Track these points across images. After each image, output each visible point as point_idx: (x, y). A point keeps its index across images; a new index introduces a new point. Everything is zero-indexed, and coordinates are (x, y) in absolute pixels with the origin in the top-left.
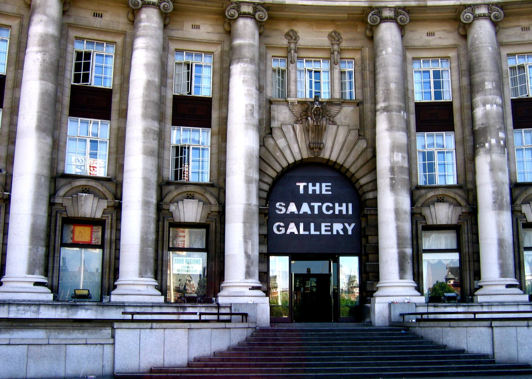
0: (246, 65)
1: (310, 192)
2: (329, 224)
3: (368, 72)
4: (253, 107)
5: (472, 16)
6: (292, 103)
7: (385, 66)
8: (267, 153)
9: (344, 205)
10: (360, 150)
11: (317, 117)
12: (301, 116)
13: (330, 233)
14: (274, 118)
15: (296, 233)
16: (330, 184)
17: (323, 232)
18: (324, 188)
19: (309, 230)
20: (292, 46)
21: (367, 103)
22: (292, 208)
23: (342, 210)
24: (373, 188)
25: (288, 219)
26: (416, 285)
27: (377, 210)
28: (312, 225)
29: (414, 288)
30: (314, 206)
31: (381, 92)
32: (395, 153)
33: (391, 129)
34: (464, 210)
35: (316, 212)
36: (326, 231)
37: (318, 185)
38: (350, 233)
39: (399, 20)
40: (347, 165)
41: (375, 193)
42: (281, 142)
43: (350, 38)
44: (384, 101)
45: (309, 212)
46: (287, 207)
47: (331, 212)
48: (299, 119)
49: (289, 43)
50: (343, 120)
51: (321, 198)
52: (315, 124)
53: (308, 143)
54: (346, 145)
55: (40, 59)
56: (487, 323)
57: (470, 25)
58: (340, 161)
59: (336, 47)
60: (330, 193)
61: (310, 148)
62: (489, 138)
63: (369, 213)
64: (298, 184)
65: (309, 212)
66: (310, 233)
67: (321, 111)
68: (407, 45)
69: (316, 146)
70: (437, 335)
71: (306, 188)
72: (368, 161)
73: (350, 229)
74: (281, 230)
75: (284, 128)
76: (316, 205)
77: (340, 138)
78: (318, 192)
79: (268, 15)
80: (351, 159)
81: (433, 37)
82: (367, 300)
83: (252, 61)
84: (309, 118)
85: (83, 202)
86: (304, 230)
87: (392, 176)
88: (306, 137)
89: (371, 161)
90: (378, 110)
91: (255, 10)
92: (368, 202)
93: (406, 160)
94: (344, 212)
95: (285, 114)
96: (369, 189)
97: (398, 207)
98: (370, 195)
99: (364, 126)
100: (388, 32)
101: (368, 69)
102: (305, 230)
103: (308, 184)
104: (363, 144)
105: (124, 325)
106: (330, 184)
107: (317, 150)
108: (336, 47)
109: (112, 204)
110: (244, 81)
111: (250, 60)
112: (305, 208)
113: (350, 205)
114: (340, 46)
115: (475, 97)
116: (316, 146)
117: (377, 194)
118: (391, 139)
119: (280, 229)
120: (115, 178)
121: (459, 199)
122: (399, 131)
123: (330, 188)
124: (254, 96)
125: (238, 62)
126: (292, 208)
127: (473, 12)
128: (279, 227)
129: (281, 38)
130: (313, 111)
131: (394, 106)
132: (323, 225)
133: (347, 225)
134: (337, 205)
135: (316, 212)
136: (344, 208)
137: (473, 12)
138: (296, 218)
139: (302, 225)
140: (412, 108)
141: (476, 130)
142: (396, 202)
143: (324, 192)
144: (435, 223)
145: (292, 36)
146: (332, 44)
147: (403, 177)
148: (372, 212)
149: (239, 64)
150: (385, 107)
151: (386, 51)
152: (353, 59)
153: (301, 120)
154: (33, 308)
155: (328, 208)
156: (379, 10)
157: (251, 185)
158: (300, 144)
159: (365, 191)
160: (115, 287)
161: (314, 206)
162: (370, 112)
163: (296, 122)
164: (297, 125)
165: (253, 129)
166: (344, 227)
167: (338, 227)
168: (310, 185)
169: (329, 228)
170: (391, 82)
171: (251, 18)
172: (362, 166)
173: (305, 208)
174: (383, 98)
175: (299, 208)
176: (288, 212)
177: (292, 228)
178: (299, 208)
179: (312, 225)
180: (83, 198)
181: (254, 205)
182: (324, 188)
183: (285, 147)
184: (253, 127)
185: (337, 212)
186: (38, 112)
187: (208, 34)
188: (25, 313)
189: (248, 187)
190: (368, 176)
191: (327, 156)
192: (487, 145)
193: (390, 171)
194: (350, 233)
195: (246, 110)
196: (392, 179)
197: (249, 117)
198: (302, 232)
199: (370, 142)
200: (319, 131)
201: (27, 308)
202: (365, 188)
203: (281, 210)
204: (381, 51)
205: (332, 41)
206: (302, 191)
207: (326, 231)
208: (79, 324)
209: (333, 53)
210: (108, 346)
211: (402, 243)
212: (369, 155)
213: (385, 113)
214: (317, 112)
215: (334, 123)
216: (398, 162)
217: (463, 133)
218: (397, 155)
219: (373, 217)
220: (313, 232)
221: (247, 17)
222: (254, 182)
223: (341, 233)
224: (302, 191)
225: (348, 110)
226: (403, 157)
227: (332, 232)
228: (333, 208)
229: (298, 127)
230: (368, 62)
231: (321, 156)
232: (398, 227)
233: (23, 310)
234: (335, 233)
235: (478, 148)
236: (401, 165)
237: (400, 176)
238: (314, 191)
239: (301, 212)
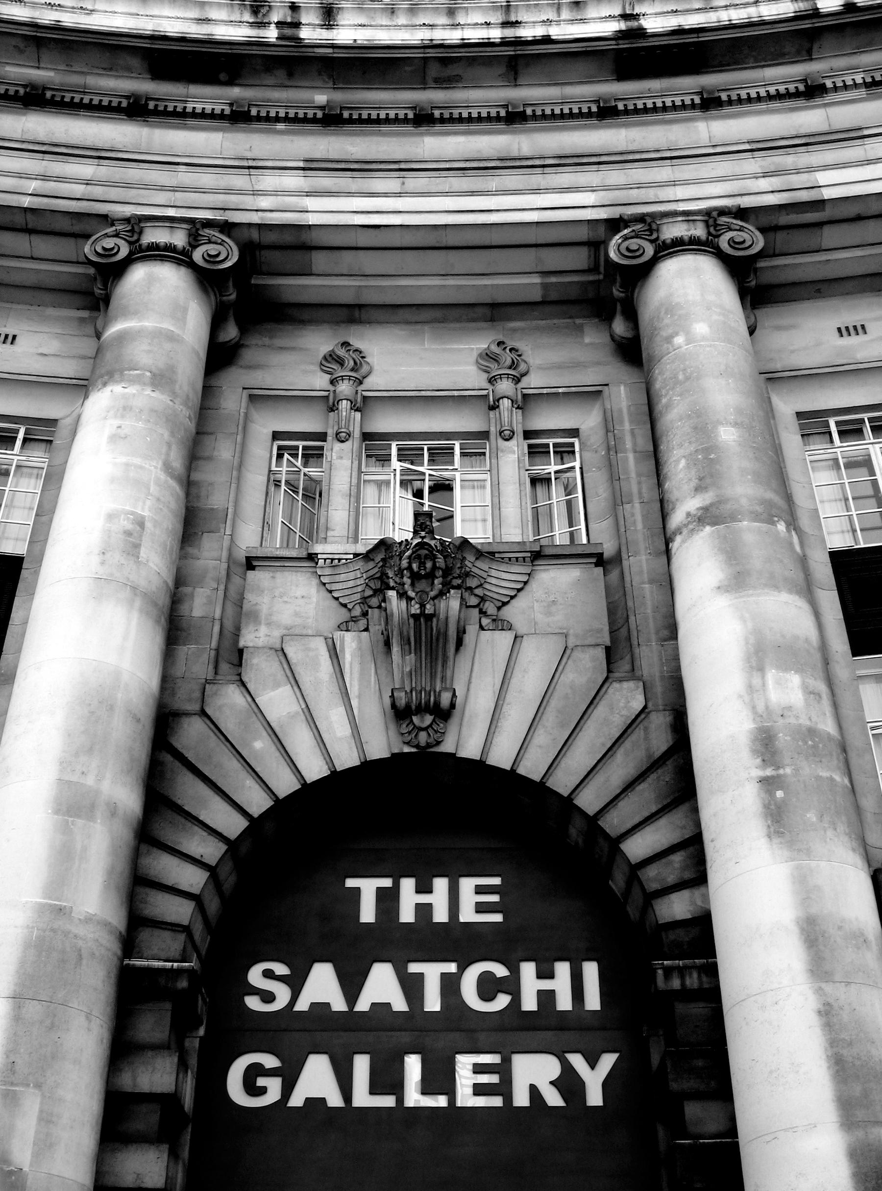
0: (132, 390)
1: (407, 915)
3: (631, 456)
4: (141, 523)
6: (334, 562)
7: (687, 379)
8: (213, 741)
9: (563, 969)
11: (422, 585)
13: (496, 1102)
14: (254, 617)
16: (496, 881)
17: (466, 1098)
19: (397, 1088)
21: (636, 554)
22: (323, 985)
23: (552, 993)
24: (688, 875)
25: (297, 1035)
27: (712, 971)
28: (413, 1065)
30: (421, 976)
31: (683, 463)
32: (771, 675)
33: (738, 580)
35: (433, 1002)
36: (479, 1090)
37: (441, 885)
38: (595, 1098)
40: (562, 783)
41: (697, 892)
42: (278, 702)
43: (556, 358)
44: (699, 489)
47: (502, 1001)
48: (357, 611)
50: (539, 617)
51: (455, 942)
52: (415, 609)
54: (555, 703)
58: (532, 768)
60: (498, 918)
61: (401, 714)
63: (676, 984)
64: (351, 883)
65: (400, 1004)
66: (400, 1100)
67: (440, 561)
68: (771, 367)
69: (422, 710)
71: (388, 900)
72: (655, 765)
73: (594, 1081)
74: (263, 1091)
75: (290, 651)
76: (432, 973)
77: (530, 680)
78: (441, 915)
79: (237, 244)
80: (580, 758)
81: (862, 338)
83: (161, 379)
86: (375, 1089)
87: (769, 772)
89: (670, 764)
90: (678, 531)
91: (195, 240)
93: (826, 704)
94: (564, 1003)
95: (301, 602)
96: (672, 879)
97: (814, 910)
98: (677, 907)
99: (629, 638)
100: (691, 295)
101: (629, 445)
103: (396, 887)
104: (627, 699)
106: (496, 881)
107: (428, 719)
108: (505, 386)
110: (114, 438)
111: (154, 375)
113: (591, 971)
114: (522, 384)
116: (422, 710)
117: (706, 898)
118: (743, 619)
119: (261, 1082)
122: (776, 587)
123: (495, 898)
124: (153, 488)
126: (323, 985)
128: (253, 1072)
129: (305, 372)
130: (405, 563)
131: (744, 502)
132: (464, 1063)
133: (577, 1061)
134: (528, 970)
135: (433, 1002)
138: (335, 1033)
139: (362, 1065)
140: (824, 571)
142: (805, 889)
143: (468, 915)
145: (344, 363)
146: (492, 381)
147: (825, 774)
148: (693, 981)
149: (108, 389)
150: (706, 509)
151: (688, 333)
153: (365, 614)
155: (488, 987)
156: (648, 223)
157: (80, 822)
158: (355, 703)
161: (421, 976)
162: (651, 581)
163: (344, 627)
164: (348, 636)
165: (131, 603)
166: (568, 1070)
167: (535, 1073)
168: (408, 885)
169: (494, 1079)
170: (719, 422)
171: (179, 262)
172: (629, 787)
173: (382, 986)
174: (694, 483)
175: (352, 985)
177: (317, 1079)
178: (352, 985)
179: (413, 1065)
181: (88, 920)
182: (468, 899)
183: (292, 716)
184: (127, 593)
185: (529, 1003)
187: (41, 358)
189: (65, 829)
190: (663, 822)
191: (470, 750)
193: (755, 752)
194: (595, 1098)
195: (108, 533)
196: (768, 784)
197: (116, 557)
198: (362, 1098)
199: (659, 689)
200: (432, 644)
202: (653, 876)
203: (268, 997)
204: (669, 339)
206: (368, 914)
207: (479, 1090)
211: (866, 1094)
212: (660, 740)
213: (708, 529)
214: (422, 564)
215: (501, 625)
216: (790, 708)
218: (778, 682)
219: (698, 1009)
220: (414, 1098)
221: (162, 259)
222: (100, 813)
223: (553, 1099)
224: (368, 914)
225: (557, 581)
226: (809, 692)
227: (508, 1096)
228: (512, 986)
229: (351, 644)
230: (627, 426)
231: (447, 747)
232: (828, 1014)
234: (521, 1099)
236: (804, 721)
237: (808, 769)
238: (424, 911)
239: (363, 1005)
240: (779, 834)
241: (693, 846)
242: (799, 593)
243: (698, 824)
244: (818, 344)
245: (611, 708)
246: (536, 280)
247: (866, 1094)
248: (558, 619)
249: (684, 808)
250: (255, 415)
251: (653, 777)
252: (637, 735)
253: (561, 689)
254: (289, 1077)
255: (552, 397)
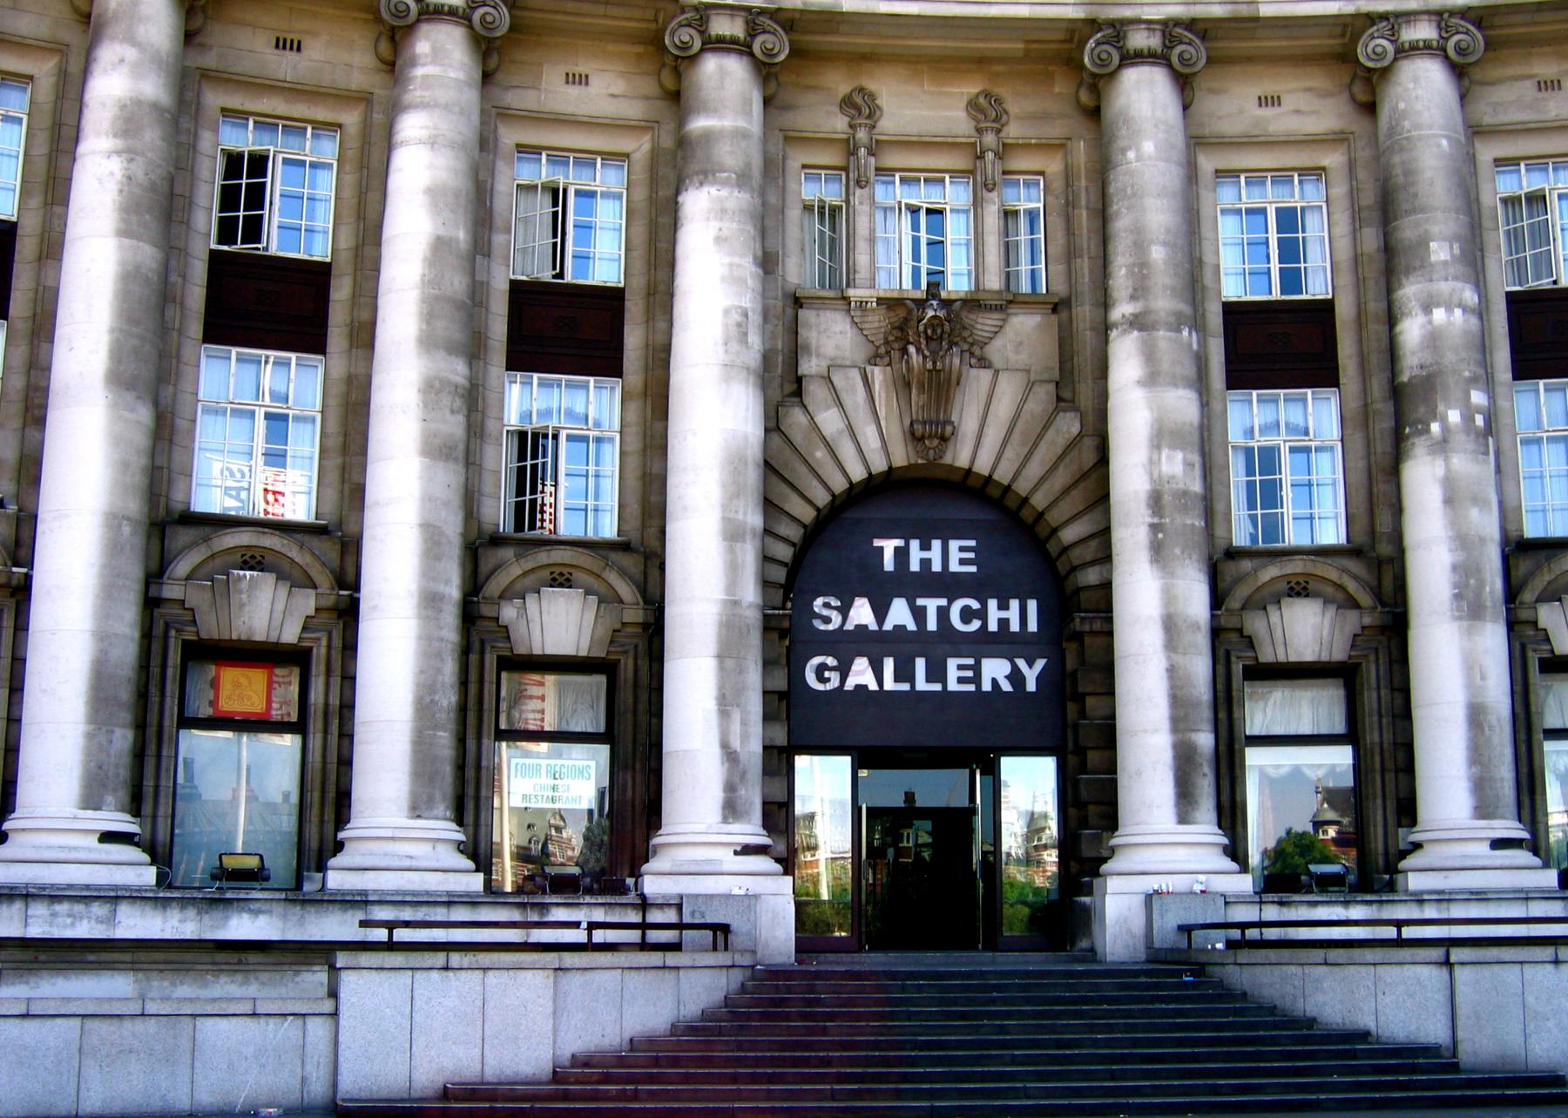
0: (725, 192)
1: (915, 566)
2: (971, 661)
3: (1084, 213)
4: (746, 315)
5: (1390, 48)
6: (862, 304)
7: (1134, 195)
8: (788, 452)
9: (1014, 604)
10: (1061, 442)
11: (934, 345)
12: (887, 342)
13: (971, 688)
14: (807, 349)
15: (873, 686)
16: (972, 543)
17: (953, 685)
18: (955, 555)
20: (862, 135)
21: (1082, 304)
22: (862, 613)
25: (848, 645)
26: (1225, 841)
27: (1110, 620)
28: (920, 664)
29: (1219, 850)
30: (924, 608)
31: (1123, 271)
32: (1165, 452)
33: (1151, 379)
34: (1367, 621)
35: (932, 625)
36: (961, 680)
37: (936, 544)
38: (1031, 686)
39: (1175, 60)
40: (1022, 487)
41: (1105, 568)
42: (829, 420)
43: (1031, 111)
45: (912, 626)
46: (844, 611)
47: (976, 625)
48: (882, 350)
49: (851, 126)
50: (1011, 355)
51: (947, 585)
52: (929, 365)
53: (907, 422)
54: (1019, 426)
55: (119, 175)
56: (1436, 953)
57: (1385, 72)
58: (1003, 475)
59: (989, 139)
60: (973, 569)
61: (914, 437)
62: (1441, 408)
63: (1087, 628)
64: (877, 543)
65: (911, 626)
67: (947, 327)
68: (1198, 133)
69: (931, 431)
70: (1289, 989)
71: (902, 555)
72: (1084, 476)
73: (1031, 676)
74: (829, 680)
75: (836, 379)
76: (932, 605)
77: (1003, 408)
78: (937, 567)
80: (1035, 470)
82: (1082, 885)
83: (742, 180)
84: (912, 349)
85: (244, 596)
86: (897, 679)
87: (1156, 520)
88: (902, 404)
89: (1094, 476)
90: (1115, 325)
91: (753, 30)
92: (1084, 596)
93: (1197, 472)
94: (1015, 626)
96: (1089, 558)
97: (1172, 610)
98: (1091, 576)
99: (1072, 373)
100: (1144, 96)
101: (1083, 202)
102: (898, 678)
103: (907, 544)
104: (1069, 425)
105: (365, 958)
106: (972, 543)
107: (936, 442)
108: (989, 139)
109: (329, 601)
111: (738, 176)
112: (899, 614)
113: (1032, 605)
115: (1400, 286)
116: (931, 431)
117: (1110, 572)
118: (1151, 409)
119: (827, 674)
120: (340, 525)
121: (1352, 586)
122: (1176, 386)
123: (972, 555)
124: (750, 282)
125: (701, 184)
126: (862, 613)
127: (1393, 36)
128: (821, 669)
129: (829, 113)
130: (921, 328)
131: (1162, 314)
132: (952, 664)
133: (1021, 663)
134: (992, 604)
135: (932, 625)
136: (1013, 614)
137: (1393, 36)
138: (873, 644)
139: (889, 665)
141: (1404, 385)
142: (1168, 597)
143: (954, 567)
144: (1282, 658)
145: (860, 107)
146: (979, 131)
147: (1189, 522)
148: (1097, 626)
149: (705, 189)
150: (1136, 316)
151: (1138, 150)
152: (1042, 173)
153: (888, 353)
154: (98, 909)
155: (967, 614)
156: (1118, 29)
158: (883, 423)
159: (1076, 562)
160: (339, 847)
161: (924, 608)
162: (1092, 329)
163: (874, 359)
164: (877, 370)
165: (747, 381)
166: (1015, 668)
167: (995, 670)
168: (915, 544)
169: (970, 674)
171: (741, 53)
172: (1066, 491)
173: (899, 614)
174: (1130, 290)
175: (880, 612)
176: (849, 626)
177: (861, 674)
178: (880, 612)
179: (920, 664)
180: (244, 585)
181: (750, 606)
182: (956, 556)
184: (744, 373)
185: (993, 626)
186: (112, 331)
188: (73, 925)
190: (1086, 518)
191: (962, 461)
192: (1435, 427)
193: (1149, 505)
194: (1031, 686)
195: (726, 325)
196: (1155, 528)
197: (735, 346)
198: (889, 684)
199: (1090, 418)
200: (941, 387)
201: (79, 908)
202: (1077, 555)
203: (827, 620)
204: (1124, 151)
205: (978, 122)
206: (889, 563)
207: (961, 680)
208: (233, 957)
209: (981, 157)
210: (318, 1020)
211: (1186, 716)
212: (1089, 458)
213: (1136, 333)
214: (934, 331)
215: (984, 363)
216: (1173, 477)
217: (1365, 391)
218: (1169, 458)
220: (922, 685)
221: (729, 51)
222: (748, 537)
223: (1006, 687)
224: (889, 563)
225: (1025, 325)
226: (1188, 465)
227: (979, 685)
228: (982, 615)
229: (878, 375)
230: (1083, 182)
231: (947, 460)
232: (1172, 671)
233: (69, 916)
234: (987, 686)
235: (1408, 437)
236: (1181, 486)
237: (1179, 520)
238: (926, 563)
239: (888, 626)
240: (1157, 561)
241: (1104, 534)
242: (1188, 385)
243: (1109, 520)
244: (1241, 112)
245: (1057, 431)
246: (1021, 46)
247: (1186, 716)
248: (1022, 359)
249: (1101, 508)
250: (790, 152)
251: (1082, 485)
252: (1075, 453)
253: (1025, 416)
254: (844, 673)
255: (1026, 147)
